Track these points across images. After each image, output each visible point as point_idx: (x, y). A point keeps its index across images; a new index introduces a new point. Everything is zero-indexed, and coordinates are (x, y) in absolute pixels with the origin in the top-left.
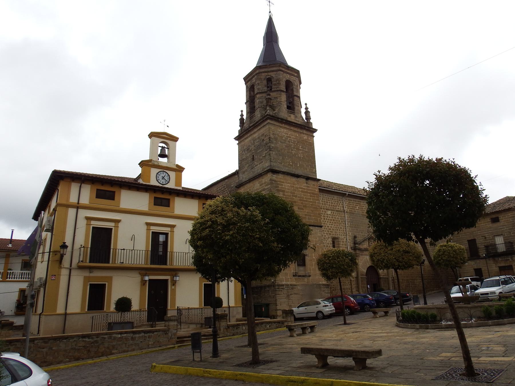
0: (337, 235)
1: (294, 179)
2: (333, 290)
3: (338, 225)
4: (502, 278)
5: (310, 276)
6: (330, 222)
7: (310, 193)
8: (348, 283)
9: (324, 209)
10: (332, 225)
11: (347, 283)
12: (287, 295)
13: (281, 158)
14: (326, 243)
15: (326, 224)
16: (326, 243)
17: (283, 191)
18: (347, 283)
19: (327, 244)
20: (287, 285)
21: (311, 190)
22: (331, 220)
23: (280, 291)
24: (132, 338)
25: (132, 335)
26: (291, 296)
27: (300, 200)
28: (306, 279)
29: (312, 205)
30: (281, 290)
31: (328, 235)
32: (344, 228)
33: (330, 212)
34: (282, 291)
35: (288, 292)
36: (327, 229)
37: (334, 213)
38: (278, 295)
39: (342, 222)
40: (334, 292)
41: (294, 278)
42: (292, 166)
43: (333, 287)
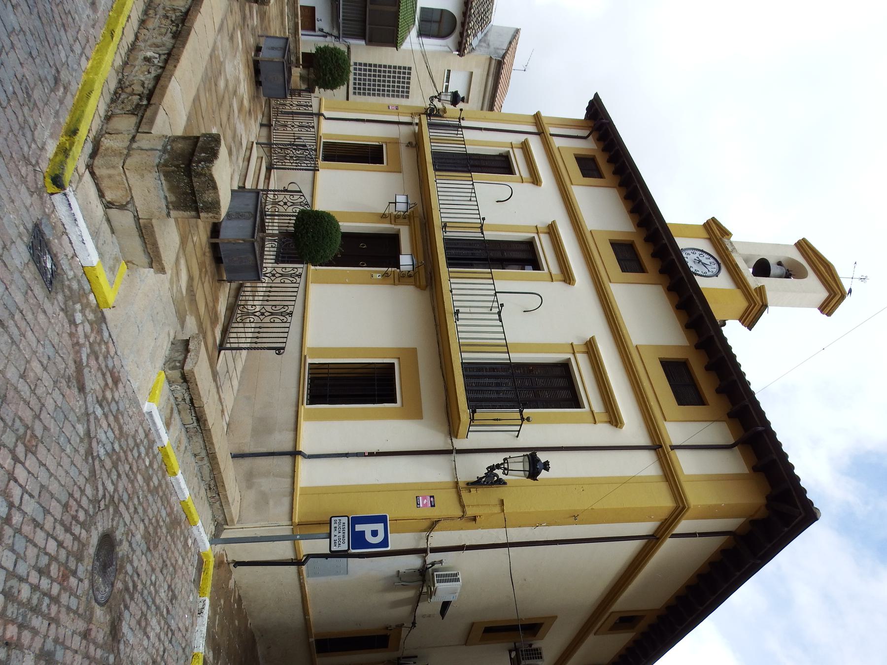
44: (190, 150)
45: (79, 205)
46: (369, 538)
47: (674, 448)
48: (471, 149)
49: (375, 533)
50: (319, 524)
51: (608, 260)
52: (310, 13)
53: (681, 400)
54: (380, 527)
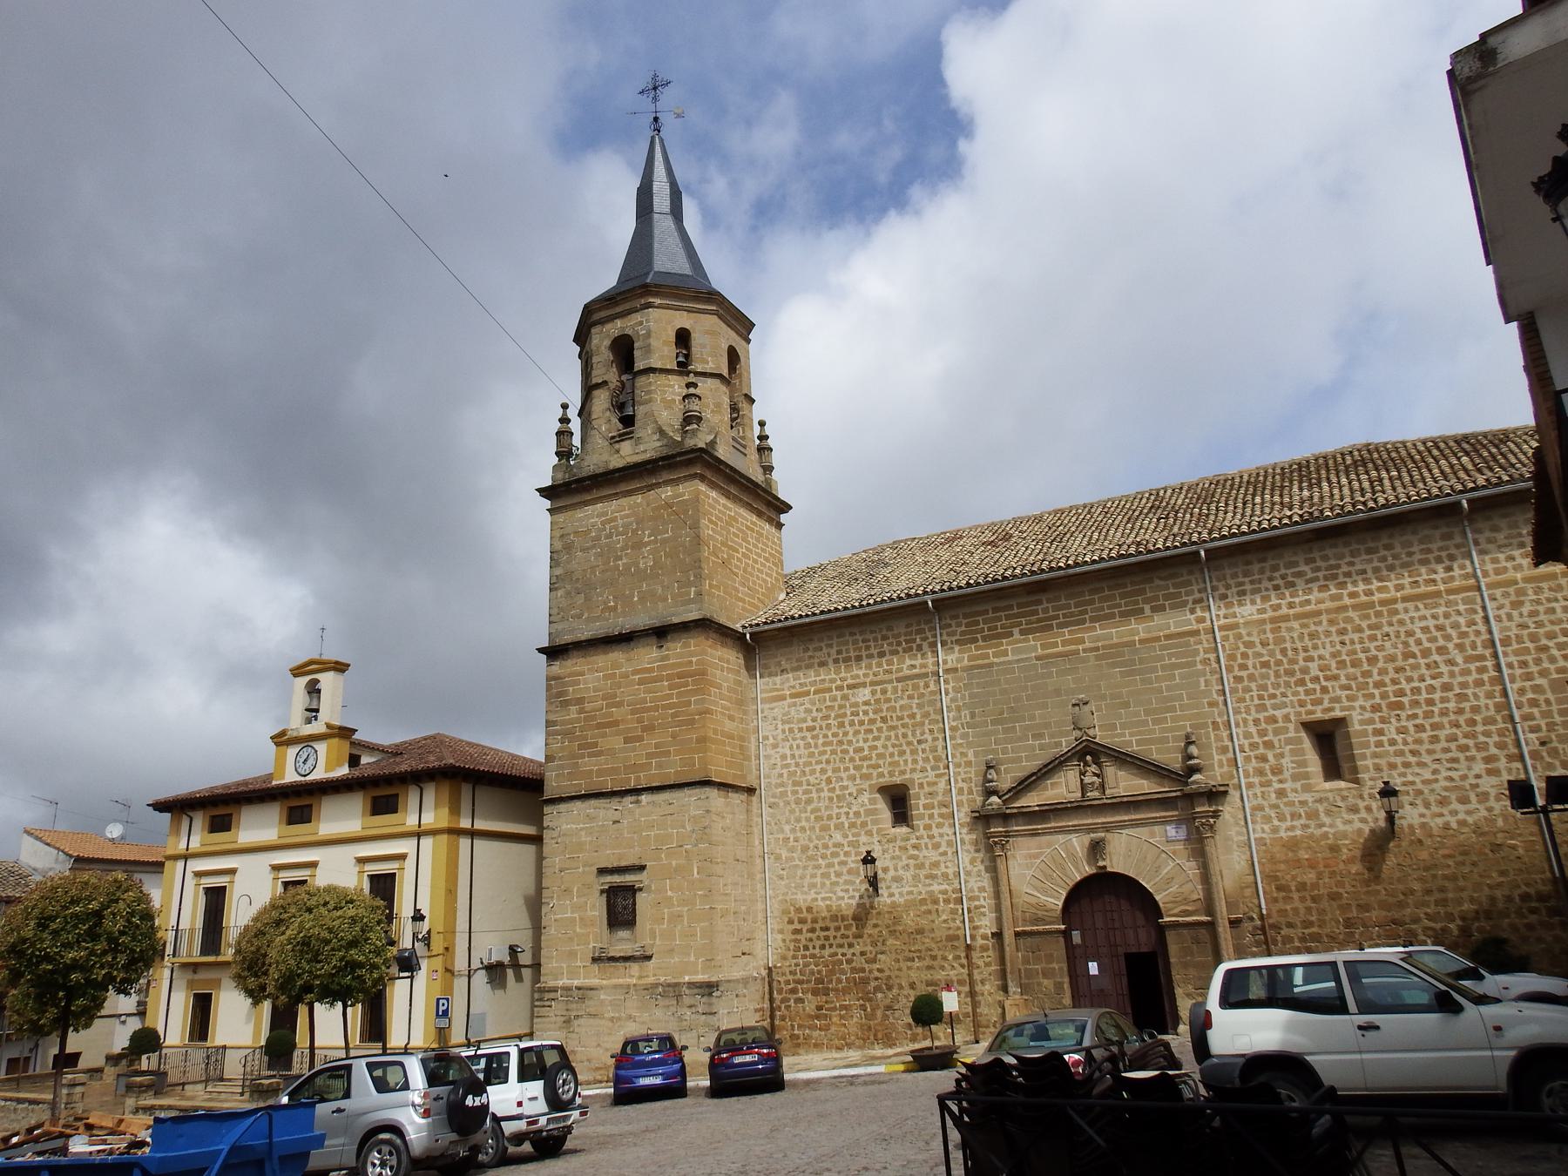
0: (903, 772)
1: (617, 656)
2: (877, 989)
3: (905, 736)
4: (460, 984)
5: (649, 958)
6: (870, 731)
7: (669, 678)
8: (957, 958)
9: (840, 688)
10: (876, 739)
11: (950, 957)
12: (563, 1019)
13: (580, 599)
14: (847, 813)
15: (850, 742)
16: (847, 813)
17: (580, 701)
18: (950, 957)
19: (851, 815)
20: (567, 989)
21: (674, 666)
22: (872, 721)
23: (544, 1006)
24: (15, 1109)
25: (14, 1104)
26: (576, 1023)
27: (633, 712)
28: (635, 968)
29: (674, 715)
30: (548, 1003)
31: (858, 781)
32: (935, 739)
33: (867, 691)
34: (550, 1006)
35: (567, 1010)
36: (852, 760)
37: (884, 692)
38: (539, 1020)
39: (926, 715)
40: (879, 995)
41: (596, 967)
42: (614, 609)
43: (876, 979)
44: (1000, 983)
45: (823, 1078)
46: (445, 1008)
47: (187, 849)
48: (199, 923)
49: (443, 1005)
50: (440, 1032)
51: (300, 831)
52: (13, 1064)
53: (394, 810)
54: (441, 1002)
